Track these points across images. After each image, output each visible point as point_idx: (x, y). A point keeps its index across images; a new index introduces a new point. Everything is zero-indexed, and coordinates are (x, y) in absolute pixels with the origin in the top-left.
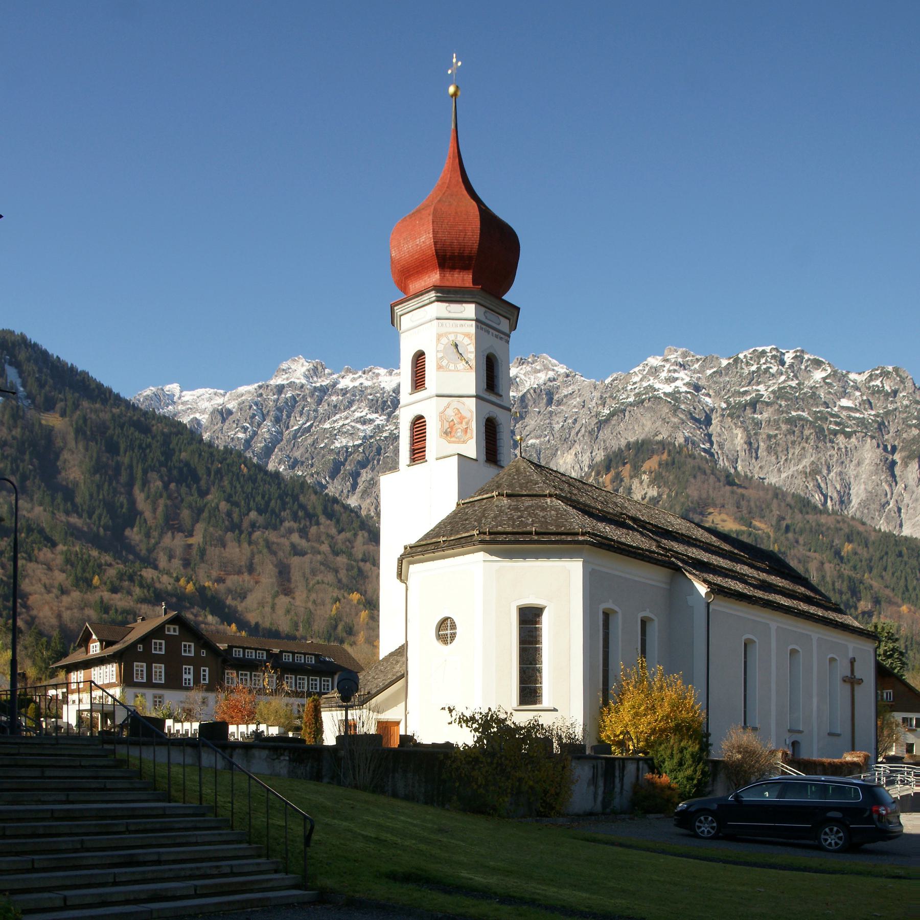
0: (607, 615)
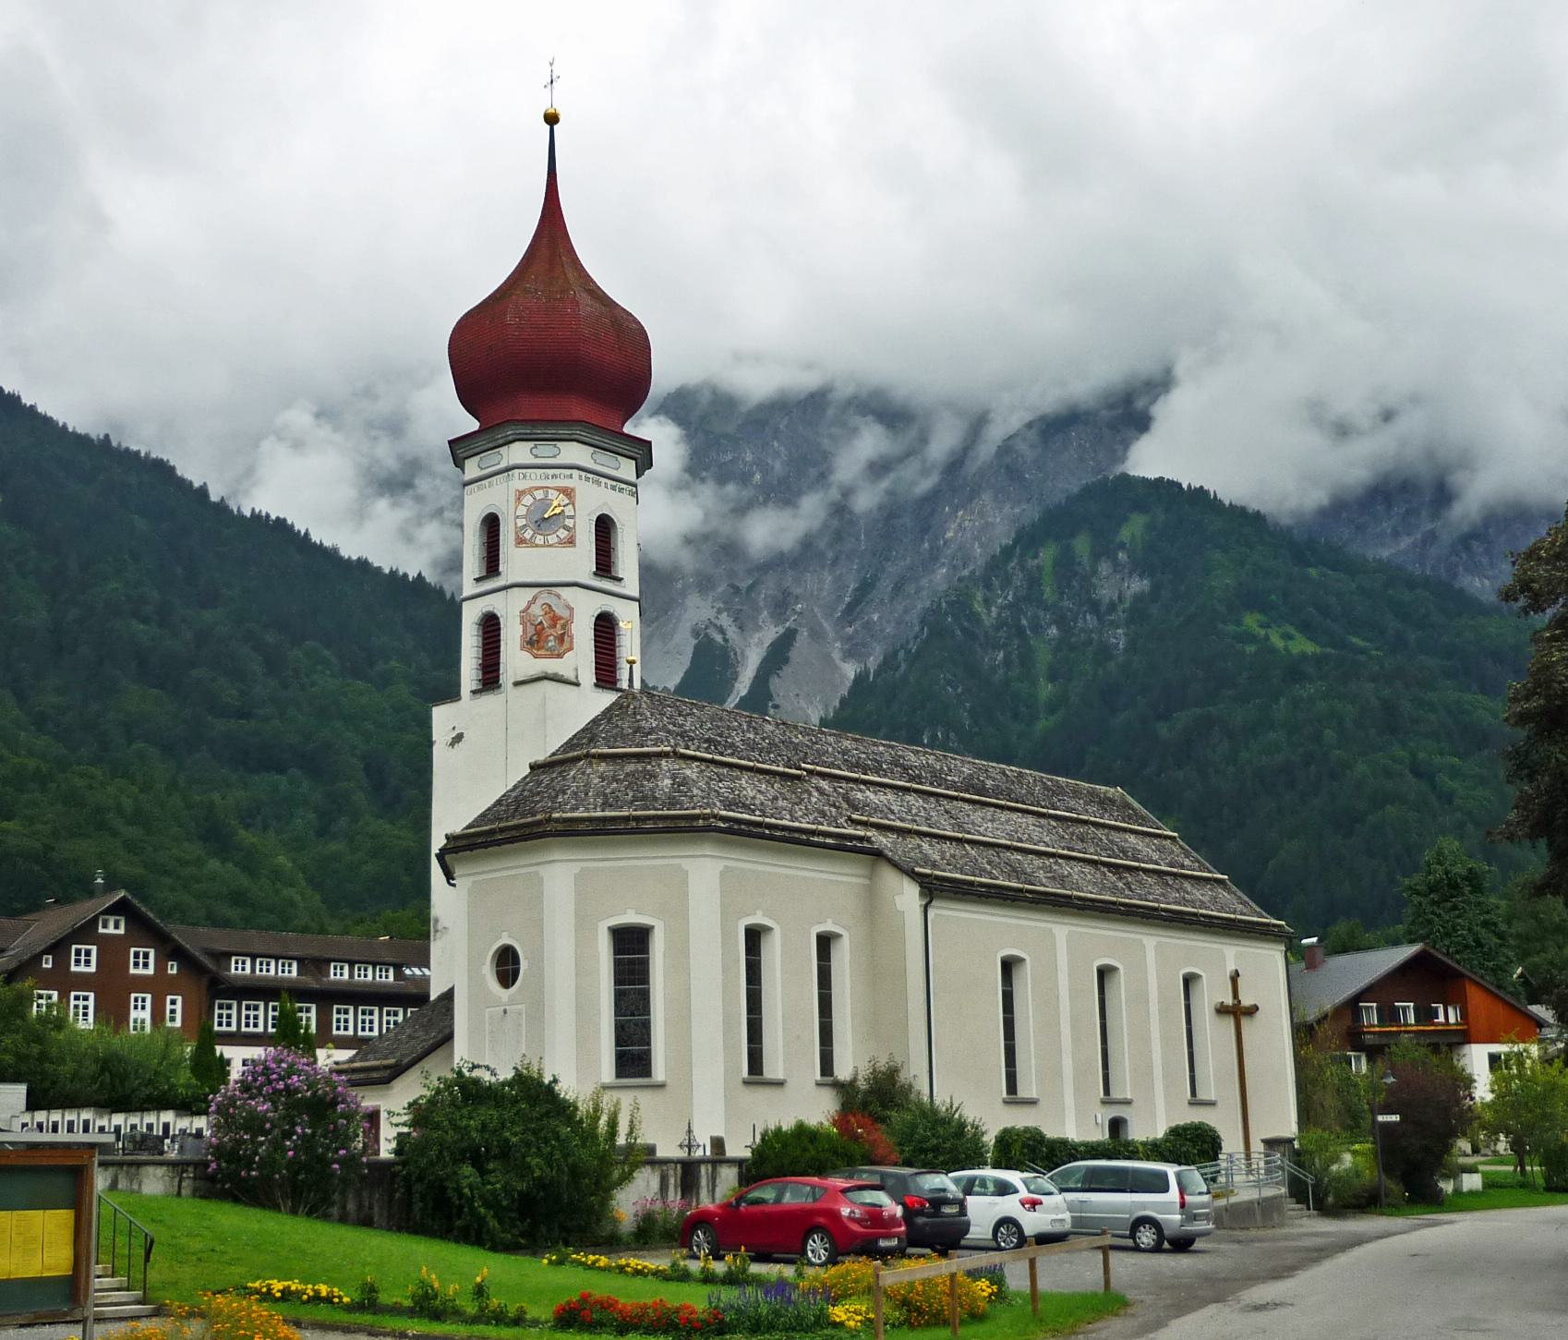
0: (754, 937)
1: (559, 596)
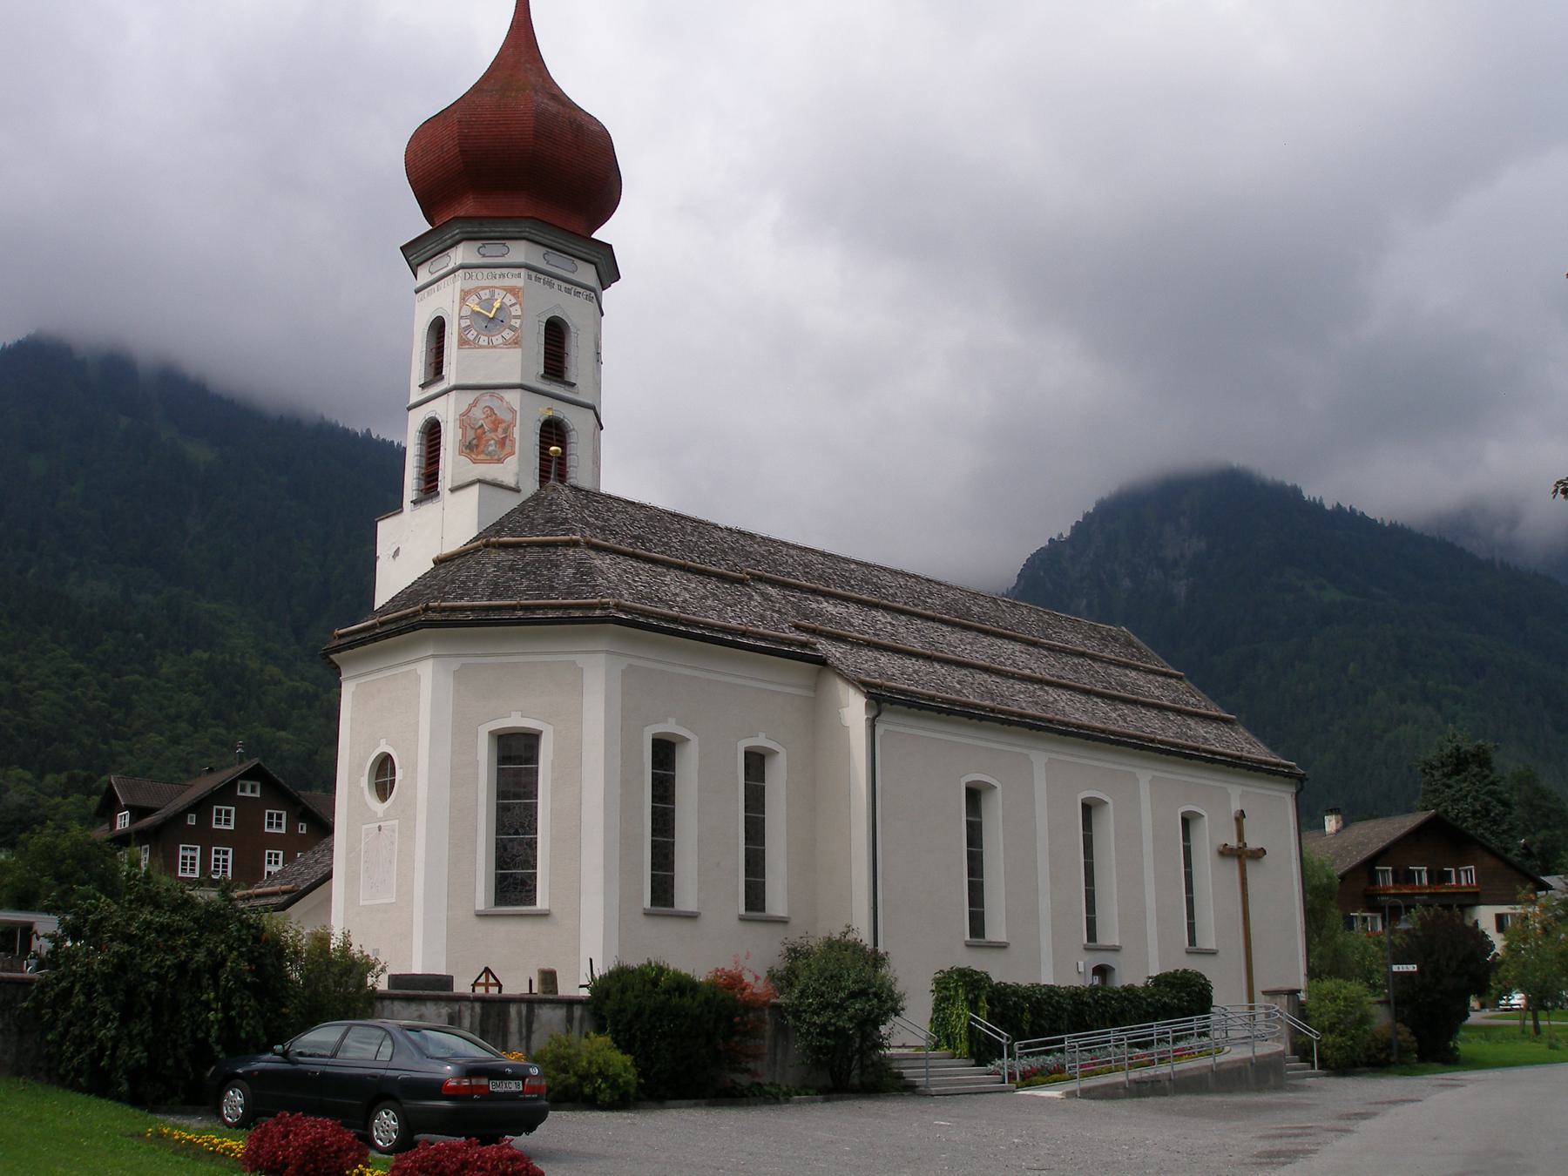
0: (664, 752)
1: (501, 399)
